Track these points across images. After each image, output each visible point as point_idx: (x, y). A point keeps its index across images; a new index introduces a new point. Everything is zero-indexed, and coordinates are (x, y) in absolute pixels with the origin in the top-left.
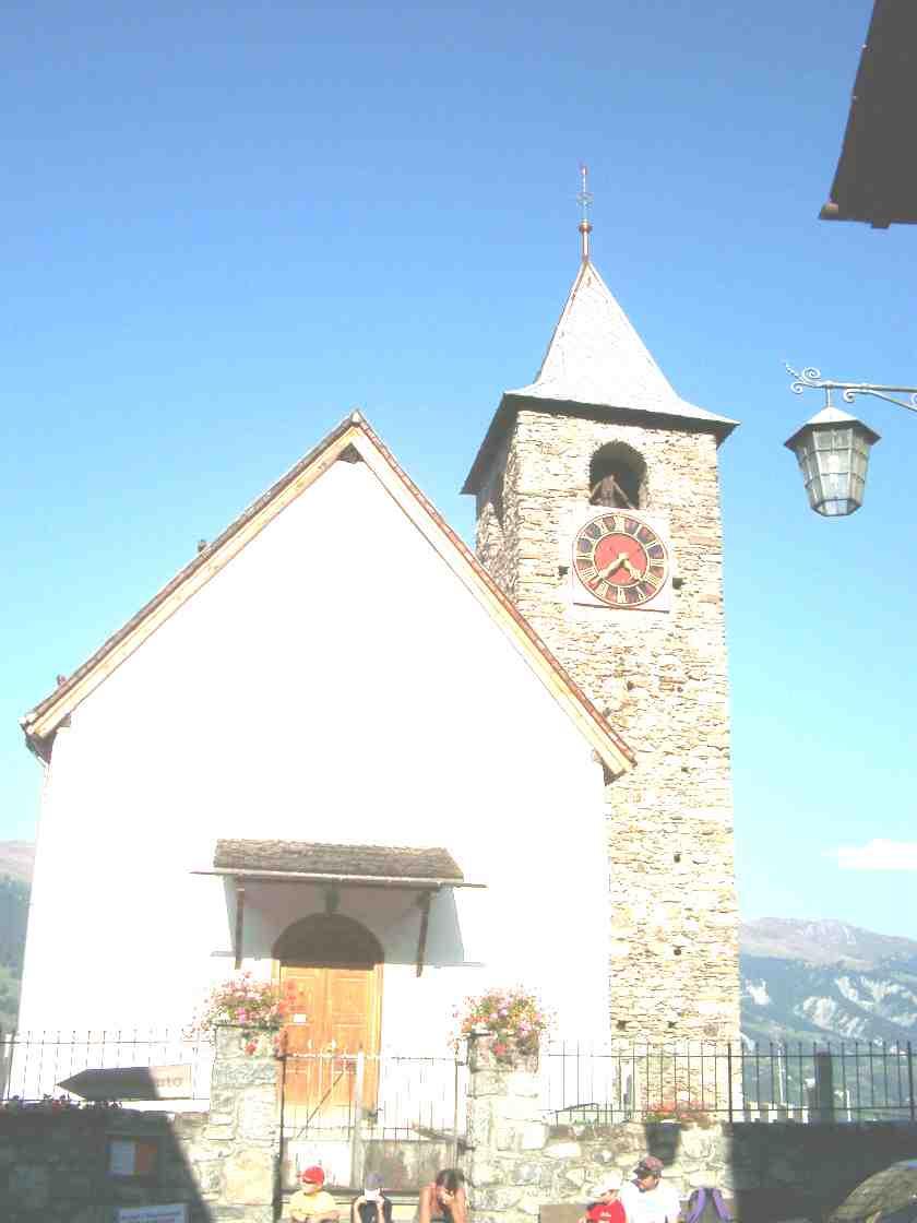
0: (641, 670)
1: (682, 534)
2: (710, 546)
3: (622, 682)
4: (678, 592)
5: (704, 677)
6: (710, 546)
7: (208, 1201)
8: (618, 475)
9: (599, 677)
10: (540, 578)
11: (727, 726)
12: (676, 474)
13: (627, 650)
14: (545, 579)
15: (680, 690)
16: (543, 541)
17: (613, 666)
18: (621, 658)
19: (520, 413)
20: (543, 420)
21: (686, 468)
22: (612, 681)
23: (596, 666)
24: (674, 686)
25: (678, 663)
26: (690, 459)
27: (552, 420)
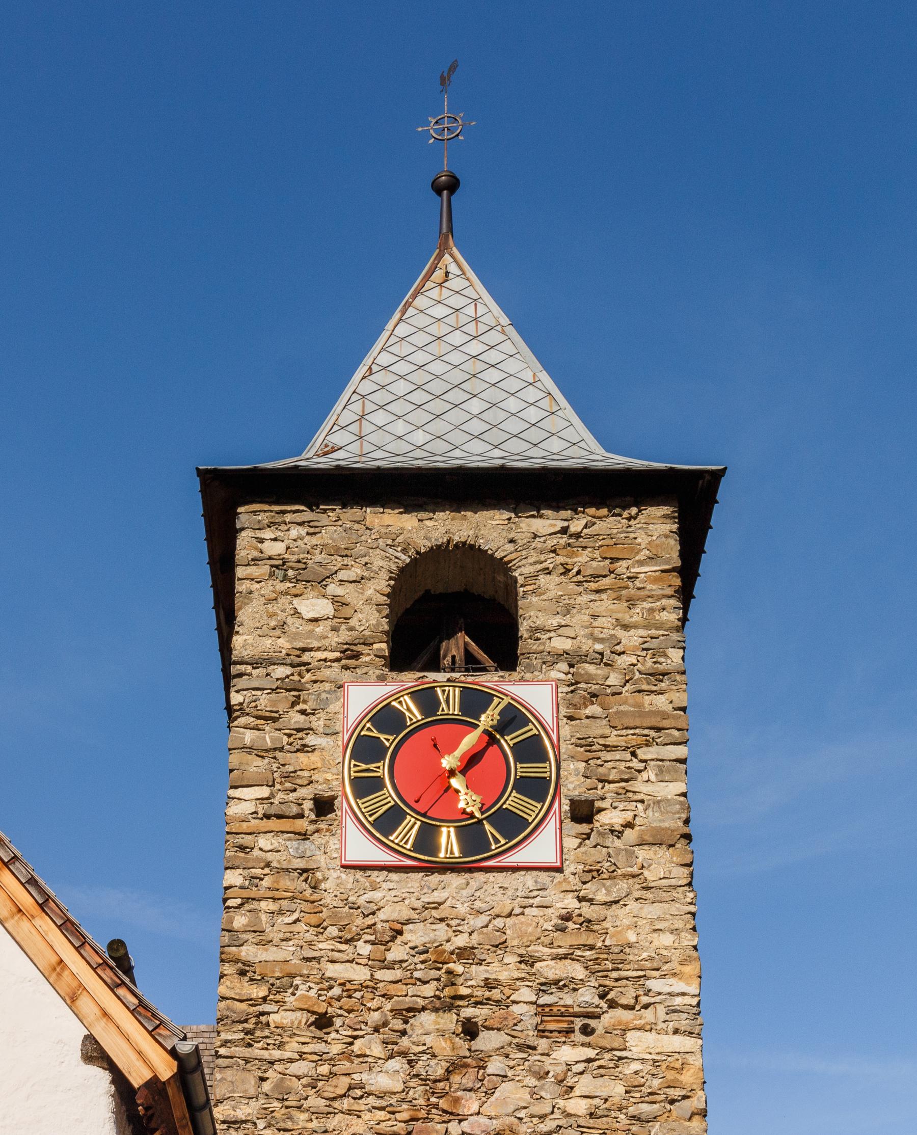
0: (496, 994)
1: (594, 709)
2: (658, 729)
3: (449, 1021)
4: (584, 828)
5: (644, 1000)
6: (658, 729)
7: (457, 640)
8: (452, 616)
9: (396, 1012)
10: (274, 824)
11: (696, 1102)
12: (586, 597)
13: (464, 953)
14: (285, 824)
15: (587, 1031)
16: (281, 749)
17: (429, 990)
18: (450, 972)
19: (240, 510)
20: (288, 517)
21: (608, 579)
22: (427, 1019)
23: (392, 989)
24: (581, 1024)
25: (578, 971)
26: (614, 560)
27: (308, 515)
